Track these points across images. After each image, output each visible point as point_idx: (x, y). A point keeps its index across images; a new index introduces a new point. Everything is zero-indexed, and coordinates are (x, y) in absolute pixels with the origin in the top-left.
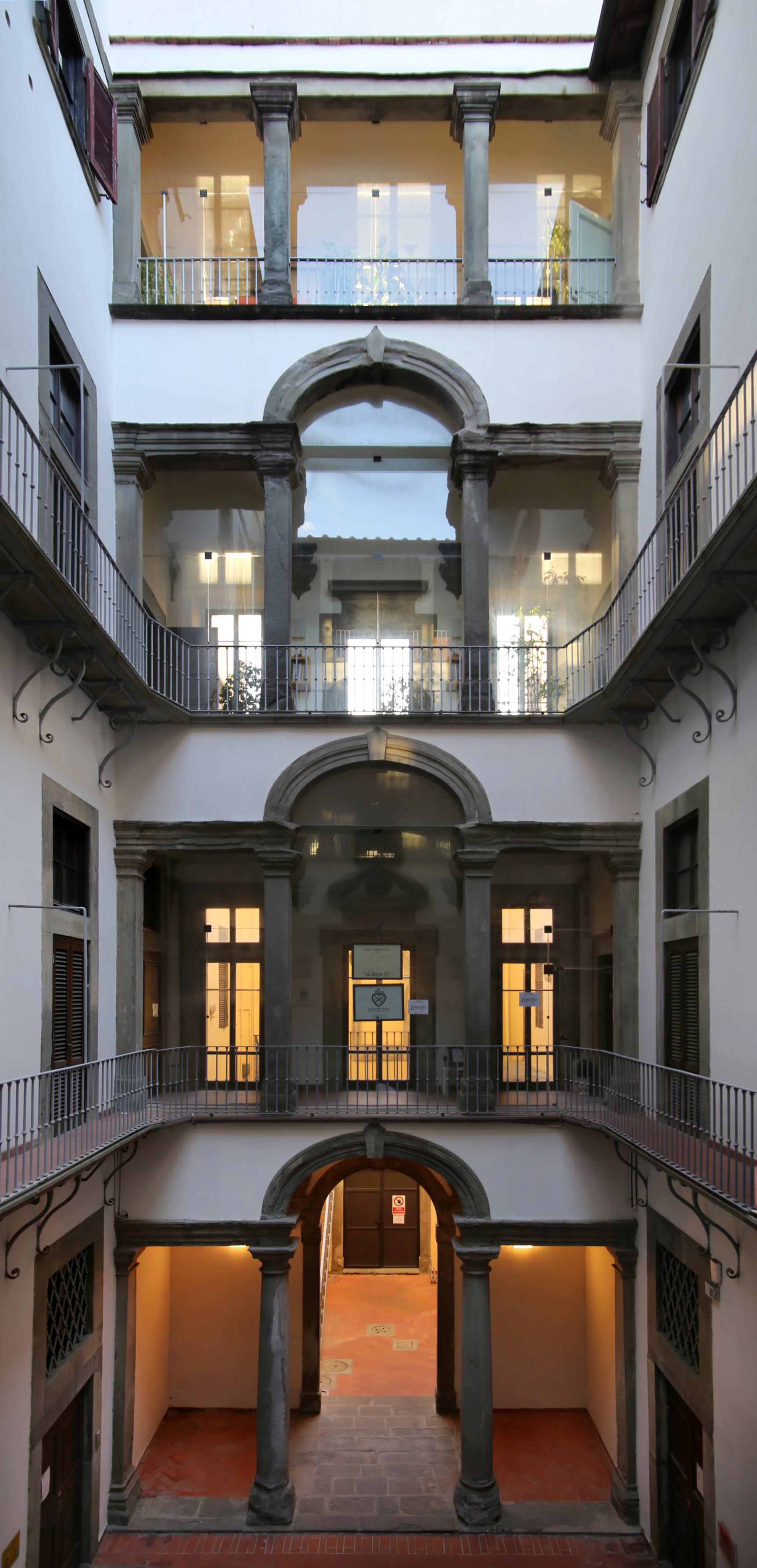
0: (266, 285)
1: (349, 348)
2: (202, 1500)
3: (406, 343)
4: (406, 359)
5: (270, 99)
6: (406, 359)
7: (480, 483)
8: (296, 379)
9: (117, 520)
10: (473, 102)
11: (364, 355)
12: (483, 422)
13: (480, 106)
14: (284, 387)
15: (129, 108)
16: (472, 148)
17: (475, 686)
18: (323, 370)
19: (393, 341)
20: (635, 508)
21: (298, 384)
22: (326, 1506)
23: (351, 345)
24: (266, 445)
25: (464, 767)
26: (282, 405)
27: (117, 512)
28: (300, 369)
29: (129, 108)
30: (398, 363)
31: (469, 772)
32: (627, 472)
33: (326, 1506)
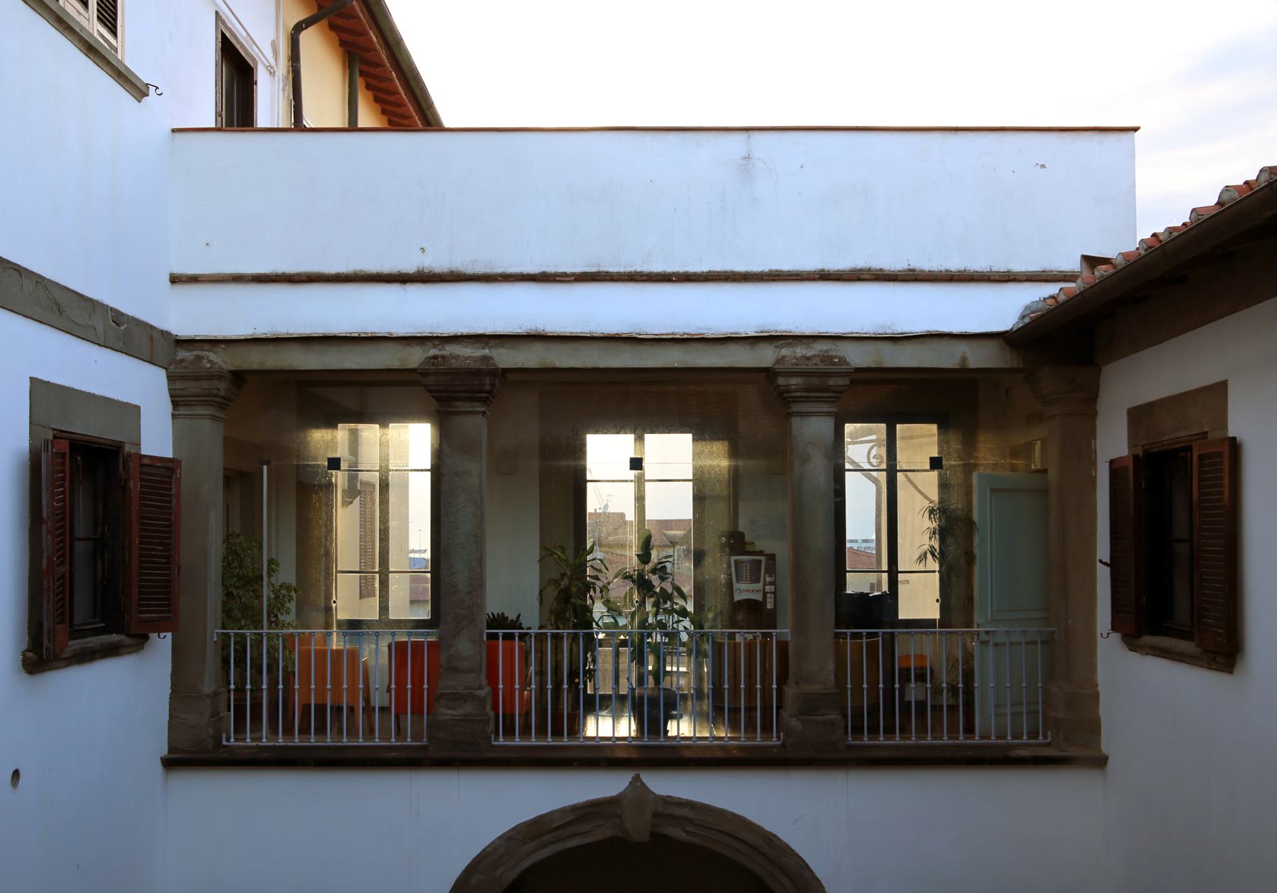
6: (691, 829)
16: (806, 459)
21: (498, 873)
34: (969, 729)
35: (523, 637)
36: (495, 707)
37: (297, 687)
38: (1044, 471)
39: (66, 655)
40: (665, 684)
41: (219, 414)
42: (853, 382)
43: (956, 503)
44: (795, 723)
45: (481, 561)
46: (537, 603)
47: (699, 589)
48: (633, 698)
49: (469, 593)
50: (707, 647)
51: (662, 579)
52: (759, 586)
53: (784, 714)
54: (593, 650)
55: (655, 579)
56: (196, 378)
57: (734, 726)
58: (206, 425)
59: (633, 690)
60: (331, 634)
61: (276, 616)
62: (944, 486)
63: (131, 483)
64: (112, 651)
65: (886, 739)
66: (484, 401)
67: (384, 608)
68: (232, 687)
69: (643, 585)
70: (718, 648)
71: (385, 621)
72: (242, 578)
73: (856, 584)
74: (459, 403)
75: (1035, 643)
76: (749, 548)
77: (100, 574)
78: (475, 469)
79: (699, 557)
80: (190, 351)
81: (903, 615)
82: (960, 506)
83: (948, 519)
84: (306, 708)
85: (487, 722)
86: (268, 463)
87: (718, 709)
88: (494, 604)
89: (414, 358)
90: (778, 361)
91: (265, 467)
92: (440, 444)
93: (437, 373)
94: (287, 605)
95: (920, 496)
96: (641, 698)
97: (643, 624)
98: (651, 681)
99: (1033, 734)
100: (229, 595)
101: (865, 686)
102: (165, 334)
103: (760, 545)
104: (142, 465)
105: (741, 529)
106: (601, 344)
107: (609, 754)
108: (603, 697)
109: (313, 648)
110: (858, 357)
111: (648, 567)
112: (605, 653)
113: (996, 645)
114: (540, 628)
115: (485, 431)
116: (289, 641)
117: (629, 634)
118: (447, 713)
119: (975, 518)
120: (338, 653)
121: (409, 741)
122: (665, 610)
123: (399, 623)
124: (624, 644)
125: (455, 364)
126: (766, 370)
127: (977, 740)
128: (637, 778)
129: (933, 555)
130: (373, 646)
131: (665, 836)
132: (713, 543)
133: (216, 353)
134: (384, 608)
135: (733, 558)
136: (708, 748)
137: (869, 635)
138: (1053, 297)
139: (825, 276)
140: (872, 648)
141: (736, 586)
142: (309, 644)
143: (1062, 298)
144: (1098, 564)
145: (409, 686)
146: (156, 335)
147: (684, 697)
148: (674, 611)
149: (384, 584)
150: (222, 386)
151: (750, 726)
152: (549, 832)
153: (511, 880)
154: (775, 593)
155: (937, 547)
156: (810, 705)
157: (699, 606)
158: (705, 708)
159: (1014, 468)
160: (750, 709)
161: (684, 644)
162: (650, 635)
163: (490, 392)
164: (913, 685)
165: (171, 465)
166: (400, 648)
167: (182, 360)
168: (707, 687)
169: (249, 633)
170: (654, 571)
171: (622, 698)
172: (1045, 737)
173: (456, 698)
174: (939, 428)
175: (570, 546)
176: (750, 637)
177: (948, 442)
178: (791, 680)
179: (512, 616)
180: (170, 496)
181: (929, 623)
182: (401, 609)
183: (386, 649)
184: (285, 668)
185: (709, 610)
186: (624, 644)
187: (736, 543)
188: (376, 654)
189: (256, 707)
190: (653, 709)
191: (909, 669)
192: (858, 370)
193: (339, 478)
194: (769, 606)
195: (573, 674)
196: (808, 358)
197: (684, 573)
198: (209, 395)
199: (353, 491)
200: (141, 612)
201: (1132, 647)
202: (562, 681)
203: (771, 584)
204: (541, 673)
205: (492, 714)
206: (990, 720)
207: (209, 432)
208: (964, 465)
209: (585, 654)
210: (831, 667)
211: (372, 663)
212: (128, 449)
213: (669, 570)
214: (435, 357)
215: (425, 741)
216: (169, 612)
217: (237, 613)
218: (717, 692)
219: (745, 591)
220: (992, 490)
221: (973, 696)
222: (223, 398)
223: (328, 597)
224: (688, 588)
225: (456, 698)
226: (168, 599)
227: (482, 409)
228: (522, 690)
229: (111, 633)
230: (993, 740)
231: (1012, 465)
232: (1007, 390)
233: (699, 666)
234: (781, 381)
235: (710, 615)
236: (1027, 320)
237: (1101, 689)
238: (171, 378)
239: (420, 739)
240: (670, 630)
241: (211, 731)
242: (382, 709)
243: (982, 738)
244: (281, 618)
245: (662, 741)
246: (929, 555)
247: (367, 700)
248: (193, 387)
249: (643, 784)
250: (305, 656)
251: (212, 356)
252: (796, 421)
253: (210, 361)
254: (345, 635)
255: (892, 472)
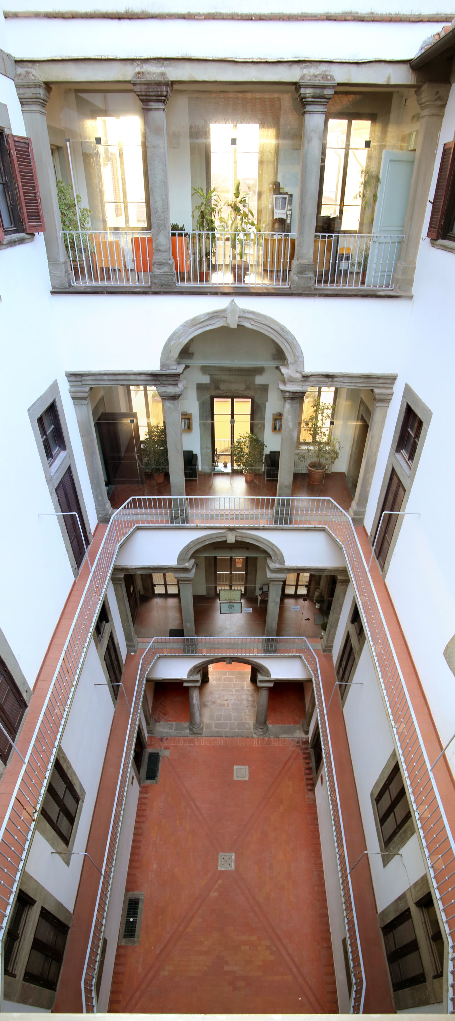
0: (155, 266)
1: (215, 315)
2: (174, 723)
3: (253, 313)
4: (253, 323)
5: (148, 94)
6: (253, 323)
7: (295, 405)
8: (180, 337)
9: (79, 425)
10: (313, 97)
11: (225, 319)
12: (299, 370)
13: (319, 100)
14: (172, 343)
15: (34, 100)
16: (310, 141)
17: (282, 511)
18: (197, 329)
19: (244, 311)
20: (383, 421)
21: (181, 340)
22: (213, 727)
23: (216, 314)
24: (163, 382)
25: (274, 545)
26: (172, 354)
27: (78, 421)
28: (181, 331)
29: (34, 100)
30: (247, 325)
31: (276, 547)
32: (382, 401)
33: (213, 727)
34: (363, 283)
35: (186, 234)
36: (176, 269)
37: (97, 259)
38: (415, 150)
39: (5, 243)
40: (244, 259)
41: (43, 110)
42: (336, 93)
43: (373, 169)
44: (295, 278)
45: (167, 195)
46: (191, 218)
47: (259, 212)
48: (232, 265)
49: (163, 212)
50: (262, 241)
51: (244, 206)
52: (285, 211)
53: (291, 273)
54: (215, 242)
55: (241, 206)
56: (29, 87)
57: (271, 278)
58: (38, 116)
59: (231, 261)
60: (107, 233)
61: (83, 225)
62: (369, 158)
63: (12, 152)
64: (21, 241)
65: (330, 286)
66: (163, 102)
67: (127, 221)
68: (71, 259)
69: (236, 209)
70: (266, 241)
71: (128, 228)
72: (67, 207)
73: (326, 212)
74: (152, 103)
75: (395, 242)
76: (281, 191)
77: (9, 202)
78: (162, 143)
79: (260, 194)
80: (22, 68)
81: (343, 228)
82: (375, 169)
83: (369, 176)
84: (102, 269)
85: (174, 275)
86: (69, 140)
87: (265, 271)
88: (173, 221)
89: (127, 73)
90: (303, 77)
91: (68, 143)
92: (145, 129)
93: (141, 84)
94: (87, 219)
95: (359, 160)
96: (235, 265)
97: (236, 229)
98: (238, 258)
99: (387, 286)
100: (63, 214)
101: (325, 261)
102: (9, 56)
103: (286, 190)
104: (15, 141)
105: (278, 181)
106: (217, 65)
107: (222, 290)
108: (219, 265)
109: (101, 240)
110: (341, 75)
111: (238, 200)
112: (220, 244)
113: (379, 243)
114: (193, 230)
115: (165, 121)
116: (91, 236)
117: (230, 234)
118: (157, 271)
119: (381, 177)
120: (111, 243)
121: (143, 284)
122: (245, 222)
123: (134, 229)
124: (228, 239)
125: (149, 78)
126: (295, 84)
127: (365, 287)
128: (233, 301)
129: (360, 196)
130: (125, 240)
131: (243, 326)
132: (267, 187)
133: (35, 70)
134: (127, 221)
135: (275, 196)
136: (261, 288)
137: (329, 237)
138: (438, 34)
139: (330, 18)
140: (330, 243)
141: (275, 211)
142: (99, 239)
143: (443, 34)
144: (428, 203)
145: (141, 259)
146: (5, 57)
147: (251, 265)
148: (249, 223)
149: (126, 208)
150: (41, 92)
151: (278, 279)
152: (199, 323)
153: (185, 343)
154: (291, 215)
155: (362, 192)
156: (302, 270)
157: (259, 221)
158: (260, 270)
159: (401, 149)
160: (278, 271)
161: (252, 240)
162: (238, 235)
163: (166, 96)
164: (344, 261)
165: (27, 141)
166: (136, 241)
167: (20, 75)
168: (261, 260)
169: (74, 233)
170: (241, 202)
171: (227, 266)
172: (392, 287)
173: (161, 264)
174: (372, 123)
175: (204, 188)
176: (279, 237)
177: (374, 132)
178: (295, 258)
179: (181, 226)
180: (30, 159)
181: (355, 232)
182: (133, 223)
183: (130, 241)
184: (91, 250)
185: (264, 223)
186: (228, 239)
187: (277, 188)
188: (126, 243)
189: (82, 268)
190: (239, 271)
191: (343, 254)
192: (339, 85)
193: (101, 148)
194: (289, 222)
195: (207, 254)
196: (316, 76)
197: (253, 204)
198: (37, 98)
199: (109, 158)
200: (29, 222)
201: (433, 245)
202: (203, 257)
203: (291, 210)
204: (194, 253)
205: (175, 272)
206: (373, 278)
207: (41, 121)
208: (380, 146)
209: (212, 243)
210: (312, 252)
211: (125, 248)
212: (7, 131)
213: (247, 202)
214: (139, 73)
215: (149, 285)
216: (40, 222)
217: (67, 223)
218: (265, 264)
219: (279, 214)
220: (390, 161)
221: (366, 268)
222: (43, 100)
223: (104, 214)
224: (255, 212)
225: (161, 264)
226: (39, 219)
227: (163, 107)
228: (187, 261)
229: (19, 232)
230: (371, 288)
231: (401, 146)
232: (406, 100)
233: (258, 250)
234: (302, 91)
235: (264, 225)
236: (423, 51)
237: (417, 265)
238: (18, 87)
239: (148, 283)
240: (247, 232)
241: (66, 279)
242: (131, 270)
243: (367, 286)
244: (86, 225)
245: (242, 285)
246: (358, 196)
247: (125, 266)
248: (29, 93)
249: (235, 304)
250: (98, 244)
251: (34, 72)
252: (307, 116)
253: (33, 75)
254: (113, 234)
255: (347, 149)
